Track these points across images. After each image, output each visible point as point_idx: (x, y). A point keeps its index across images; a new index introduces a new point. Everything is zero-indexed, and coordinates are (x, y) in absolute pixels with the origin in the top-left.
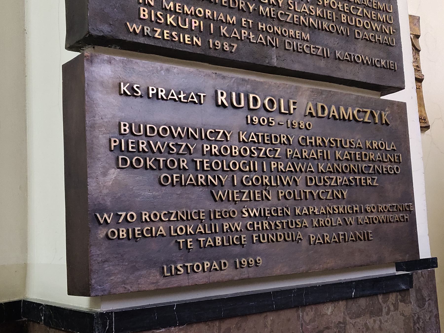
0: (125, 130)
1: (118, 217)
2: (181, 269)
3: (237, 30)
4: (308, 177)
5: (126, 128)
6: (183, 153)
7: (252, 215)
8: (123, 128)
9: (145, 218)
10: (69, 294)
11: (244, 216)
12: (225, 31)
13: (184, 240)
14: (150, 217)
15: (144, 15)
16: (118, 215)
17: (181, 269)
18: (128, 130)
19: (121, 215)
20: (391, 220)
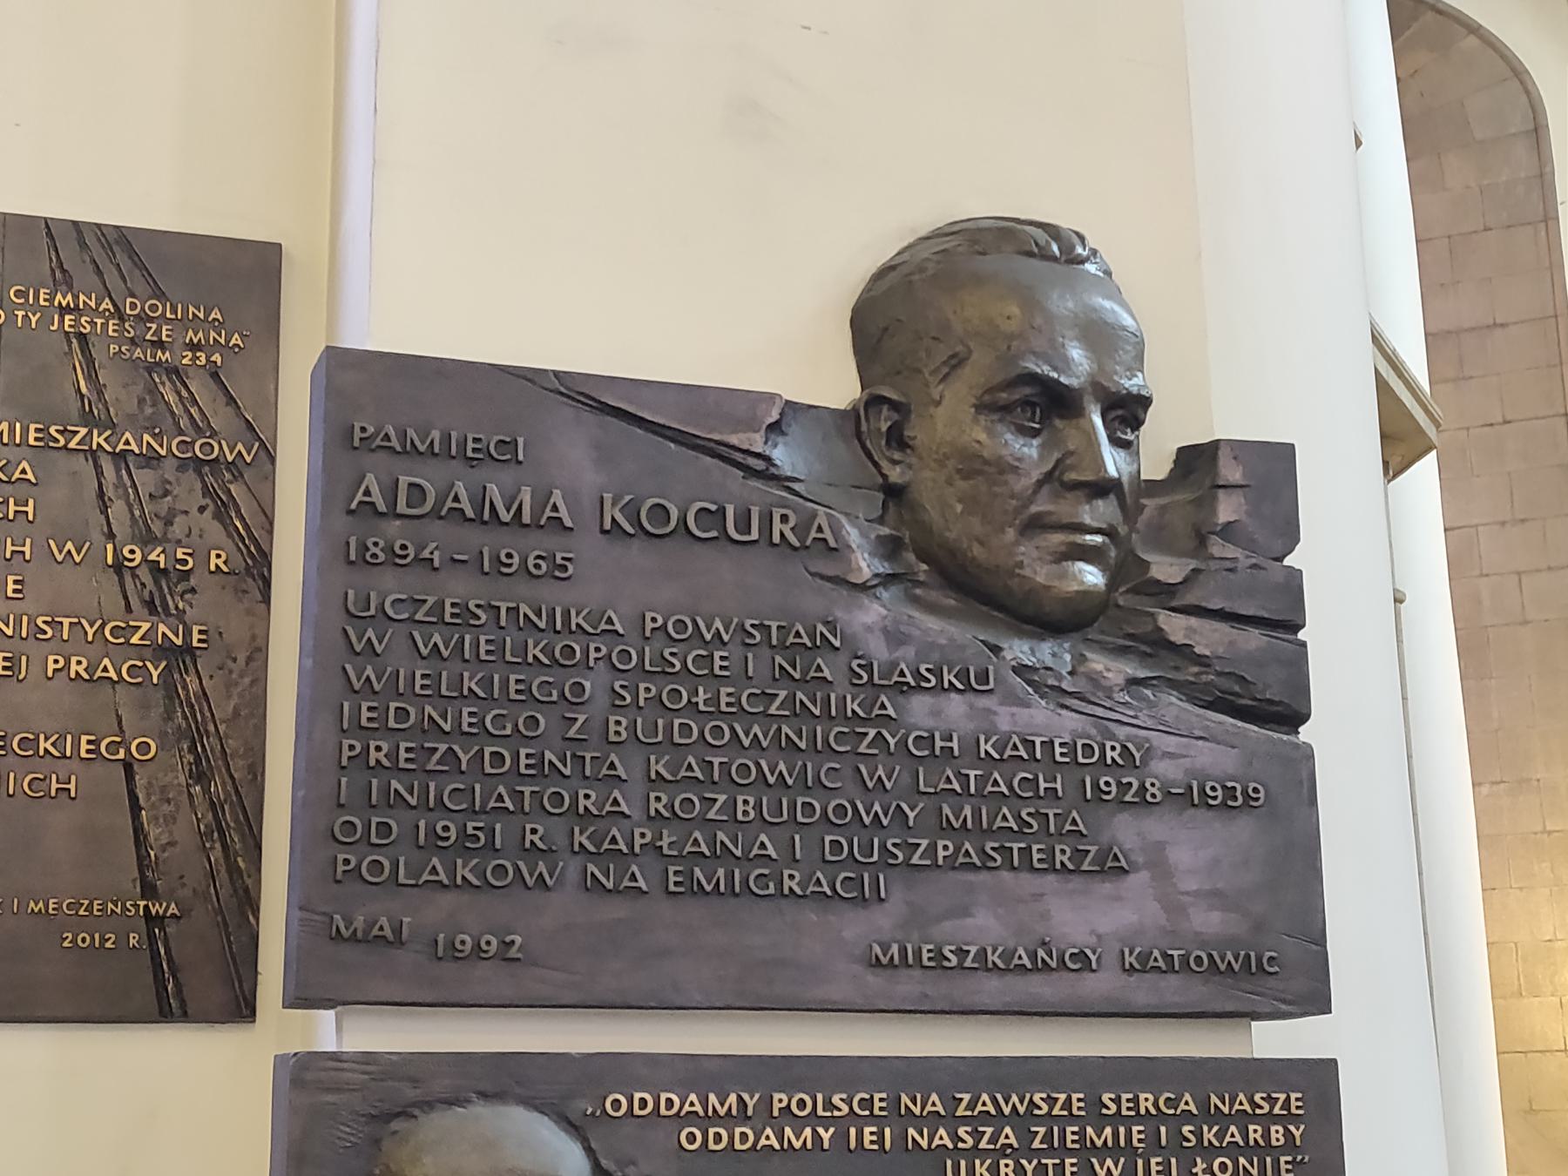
0: (745, 813)
1: (957, 1102)
2: (1262, 1103)
3: (1001, 776)
4: (404, 480)
5: (749, 809)
6: (579, 737)
7: (1007, 1111)
8: (612, 727)
9: (1146, 1108)
10: (1335, 1061)
11: (1104, 1111)
12: (1136, 959)
13: (1057, 1161)
14: (1156, 1105)
15: (1278, 1140)
16: (954, 1098)
17: (1262, 1103)
18: (752, 814)
19: (961, 1099)
20: (771, 416)
